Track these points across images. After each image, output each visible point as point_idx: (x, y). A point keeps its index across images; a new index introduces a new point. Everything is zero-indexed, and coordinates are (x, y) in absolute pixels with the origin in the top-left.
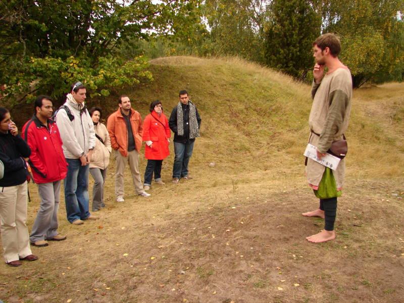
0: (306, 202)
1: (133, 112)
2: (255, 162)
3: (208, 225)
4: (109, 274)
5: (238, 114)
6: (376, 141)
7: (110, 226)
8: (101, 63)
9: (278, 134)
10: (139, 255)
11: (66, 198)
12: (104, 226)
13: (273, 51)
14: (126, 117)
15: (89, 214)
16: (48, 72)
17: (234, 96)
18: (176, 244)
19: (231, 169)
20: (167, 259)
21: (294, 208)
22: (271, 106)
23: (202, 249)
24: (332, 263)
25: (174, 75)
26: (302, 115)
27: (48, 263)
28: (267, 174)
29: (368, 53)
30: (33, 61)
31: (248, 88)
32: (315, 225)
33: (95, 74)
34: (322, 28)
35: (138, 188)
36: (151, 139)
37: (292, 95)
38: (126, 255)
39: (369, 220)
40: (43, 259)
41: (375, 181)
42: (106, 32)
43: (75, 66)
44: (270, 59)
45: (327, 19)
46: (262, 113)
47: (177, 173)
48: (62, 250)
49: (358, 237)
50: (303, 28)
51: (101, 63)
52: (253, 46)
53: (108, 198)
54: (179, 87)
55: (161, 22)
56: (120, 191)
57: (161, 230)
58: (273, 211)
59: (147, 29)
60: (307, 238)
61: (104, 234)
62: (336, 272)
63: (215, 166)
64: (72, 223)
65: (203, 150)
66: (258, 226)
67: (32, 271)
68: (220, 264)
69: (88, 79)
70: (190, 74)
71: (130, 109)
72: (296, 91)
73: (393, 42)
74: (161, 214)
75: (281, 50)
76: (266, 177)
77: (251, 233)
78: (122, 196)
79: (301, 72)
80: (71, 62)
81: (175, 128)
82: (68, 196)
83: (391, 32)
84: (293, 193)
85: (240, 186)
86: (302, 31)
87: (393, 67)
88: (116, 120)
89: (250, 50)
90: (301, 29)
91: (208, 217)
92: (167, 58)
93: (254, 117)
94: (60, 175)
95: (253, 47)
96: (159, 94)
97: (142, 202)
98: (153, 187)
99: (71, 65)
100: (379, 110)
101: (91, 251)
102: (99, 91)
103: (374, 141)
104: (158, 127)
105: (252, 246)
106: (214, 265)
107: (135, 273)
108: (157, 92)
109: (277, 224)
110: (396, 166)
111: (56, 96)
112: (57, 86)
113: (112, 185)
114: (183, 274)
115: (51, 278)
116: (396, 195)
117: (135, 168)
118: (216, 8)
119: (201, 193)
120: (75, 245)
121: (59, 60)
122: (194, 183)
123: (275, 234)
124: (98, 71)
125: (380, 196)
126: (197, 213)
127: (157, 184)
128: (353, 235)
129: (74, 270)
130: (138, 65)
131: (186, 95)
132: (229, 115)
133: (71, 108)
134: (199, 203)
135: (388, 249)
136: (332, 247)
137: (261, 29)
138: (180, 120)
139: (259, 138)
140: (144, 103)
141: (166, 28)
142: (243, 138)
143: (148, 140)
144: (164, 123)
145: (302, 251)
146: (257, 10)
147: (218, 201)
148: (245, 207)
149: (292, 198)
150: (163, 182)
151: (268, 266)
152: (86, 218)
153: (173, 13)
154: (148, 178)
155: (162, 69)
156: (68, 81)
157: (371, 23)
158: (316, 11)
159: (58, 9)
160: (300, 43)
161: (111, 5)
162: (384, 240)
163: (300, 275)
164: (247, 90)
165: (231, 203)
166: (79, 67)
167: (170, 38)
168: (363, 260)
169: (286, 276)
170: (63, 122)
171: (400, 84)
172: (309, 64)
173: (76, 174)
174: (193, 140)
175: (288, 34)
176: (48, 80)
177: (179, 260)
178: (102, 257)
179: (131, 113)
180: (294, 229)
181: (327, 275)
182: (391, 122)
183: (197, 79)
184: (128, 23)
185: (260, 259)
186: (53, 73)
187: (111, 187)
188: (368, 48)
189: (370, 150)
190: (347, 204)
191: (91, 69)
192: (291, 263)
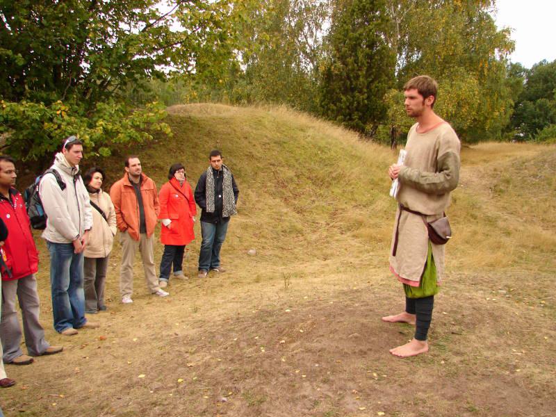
0: (386, 302)
1: (145, 179)
2: (310, 249)
3: (255, 335)
4: (121, 403)
6: (472, 220)
7: (117, 336)
8: (98, 111)
9: (341, 211)
10: (161, 377)
11: (53, 298)
12: (107, 336)
13: (332, 98)
14: (135, 186)
15: (85, 319)
16: (25, 122)
17: (281, 158)
18: (211, 360)
19: (278, 259)
20: (200, 381)
21: (371, 311)
22: (331, 172)
23: (248, 368)
24: (425, 383)
25: (198, 129)
26: (372, 186)
27: (31, 390)
28: (327, 265)
29: (458, 103)
30: (4, 106)
31: (299, 148)
32: (401, 333)
33: (92, 126)
34: (397, 68)
35: (152, 284)
36: (169, 218)
37: (360, 158)
38: (142, 376)
39: (471, 326)
40: (24, 384)
41: (476, 274)
42: (106, 68)
43: (64, 113)
44: (328, 109)
45: (403, 56)
46: (319, 182)
47: (205, 263)
48: (49, 371)
49: (458, 348)
50: (373, 68)
51: (98, 111)
52: (304, 91)
53: (110, 298)
54: (206, 146)
55: (181, 57)
56: (127, 288)
57: (189, 341)
58: (342, 315)
59: (163, 66)
60: (391, 350)
61: (108, 348)
62: (432, 396)
63: (256, 255)
64: (60, 333)
65: (239, 232)
66: (323, 336)
67: (8, 402)
68: (275, 387)
69: (82, 133)
70: (220, 128)
71: (141, 175)
72: (364, 153)
73: (490, 88)
74: (186, 319)
75: (342, 97)
76: (326, 269)
77: (314, 345)
78: (129, 297)
79: (369, 127)
80: (57, 108)
81: (203, 202)
82: (56, 296)
83: (488, 75)
84: (368, 290)
85: (293, 280)
86: (371, 72)
87: (490, 122)
88: (123, 190)
89: (300, 96)
90: (370, 68)
91: (253, 324)
92: (188, 106)
93: (309, 187)
94: (29, 267)
95: (304, 92)
96: (179, 155)
97: (158, 304)
98: (172, 283)
99: (59, 112)
100: (474, 179)
101: (92, 372)
102: (95, 149)
103: (469, 220)
104: (179, 201)
105: (318, 362)
106: (267, 389)
107: (157, 402)
108: (175, 153)
109: (349, 332)
110: (500, 253)
111: (36, 155)
112: (37, 141)
113: (114, 281)
114: (224, 401)
115: (36, 411)
116: (504, 292)
117: (150, 254)
118: (253, 38)
119: (240, 291)
120: (69, 364)
121: (42, 106)
122: (229, 278)
123: (347, 346)
124: (96, 122)
125: (484, 294)
126: (238, 319)
127: (177, 278)
128: (452, 346)
129: (70, 399)
130: (151, 114)
131: (218, 158)
132: (274, 185)
133: (61, 173)
134: (239, 305)
135: (498, 363)
136: (425, 362)
137: (316, 69)
138: (210, 192)
139: (315, 215)
140: (157, 167)
141: (189, 65)
142: (293, 217)
143: (165, 218)
144: (187, 195)
145: (385, 369)
146: (310, 41)
147: (265, 302)
148: (304, 309)
149: (366, 297)
150: (186, 275)
151: (341, 389)
152: (80, 326)
153: (199, 44)
154: (165, 270)
155: (182, 121)
156: (52, 135)
157: (461, 63)
158: (390, 45)
159: (41, 35)
160: (368, 87)
161: (113, 31)
162: (494, 352)
163: (384, 401)
164: (298, 151)
165: (283, 305)
166: (69, 115)
167: (194, 79)
168: (467, 379)
169: (366, 402)
170: (51, 190)
171: (500, 144)
172: (380, 116)
173: (68, 263)
174: (227, 219)
175: (352, 75)
176: (25, 133)
177: (217, 383)
178: (107, 380)
179: (141, 180)
180: (372, 339)
181: (421, 400)
182: (492, 195)
183: (229, 134)
184: (137, 57)
185: (329, 380)
186: (31, 124)
187: (113, 283)
188: (458, 96)
189: (464, 233)
190: (441, 304)
191: (85, 119)
192: (371, 384)
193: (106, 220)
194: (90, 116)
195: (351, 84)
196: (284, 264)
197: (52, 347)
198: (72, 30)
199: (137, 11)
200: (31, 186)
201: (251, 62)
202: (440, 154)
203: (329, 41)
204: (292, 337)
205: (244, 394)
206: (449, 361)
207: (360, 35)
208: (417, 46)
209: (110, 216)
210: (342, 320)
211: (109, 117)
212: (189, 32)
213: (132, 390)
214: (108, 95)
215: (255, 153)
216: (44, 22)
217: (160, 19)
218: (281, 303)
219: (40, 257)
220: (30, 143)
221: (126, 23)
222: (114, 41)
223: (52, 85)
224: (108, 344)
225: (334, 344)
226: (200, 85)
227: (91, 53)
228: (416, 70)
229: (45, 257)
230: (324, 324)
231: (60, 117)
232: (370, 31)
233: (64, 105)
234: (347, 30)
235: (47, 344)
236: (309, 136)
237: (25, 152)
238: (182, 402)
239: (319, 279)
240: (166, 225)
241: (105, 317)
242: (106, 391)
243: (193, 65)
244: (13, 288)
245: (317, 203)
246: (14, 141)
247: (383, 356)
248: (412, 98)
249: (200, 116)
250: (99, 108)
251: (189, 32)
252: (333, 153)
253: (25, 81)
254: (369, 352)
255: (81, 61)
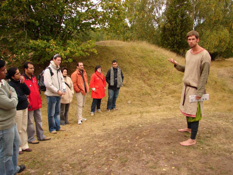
2: (154, 101)
3: (126, 135)
4: (71, 160)
5: (145, 74)
6: (223, 91)
8: (68, 44)
10: (88, 150)
12: (68, 134)
15: (60, 127)
21: (174, 127)
23: (122, 148)
26: (181, 76)
28: (160, 108)
30: (31, 42)
31: (151, 59)
32: (185, 136)
36: (95, 87)
38: (80, 150)
39: (215, 134)
40: (35, 151)
42: (71, 26)
44: (164, 43)
45: (197, 21)
46: (158, 74)
47: (110, 106)
48: (45, 146)
50: (183, 26)
51: (68, 44)
52: (154, 35)
55: (102, 21)
57: (100, 137)
58: (162, 128)
60: (180, 143)
62: (195, 162)
66: (153, 136)
67: (29, 157)
69: (61, 53)
70: (118, 51)
75: (170, 38)
76: (160, 110)
79: (181, 51)
81: (109, 81)
84: (174, 119)
85: (144, 114)
89: (152, 38)
90: (182, 26)
93: (154, 76)
94: (38, 106)
97: (89, 122)
98: (96, 114)
102: (66, 59)
103: (222, 91)
104: (99, 80)
105: (150, 147)
106: (129, 156)
112: (43, 56)
114: (111, 161)
119: (123, 118)
120: (52, 144)
121: (45, 42)
124: (67, 48)
126: (120, 129)
128: (206, 142)
130: (89, 45)
131: (116, 63)
132: (139, 75)
134: (121, 123)
135: (225, 150)
137: (159, 26)
138: (112, 77)
139: (156, 88)
143: (93, 87)
144: (102, 78)
145: (177, 150)
146: (157, 15)
147: (132, 122)
148: (147, 126)
149: (173, 121)
150: (102, 111)
151: (158, 157)
153: (109, 16)
156: (49, 53)
157: (222, 23)
161: (75, 11)
163: (175, 163)
164: (150, 61)
165: (139, 124)
166: (56, 45)
167: (107, 31)
168: (211, 156)
169: (168, 163)
173: (55, 105)
174: (119, 88)
175: (174, 29)
176: (39, 52)
177: (109, 153)
180: (173, 138)
181: (190, 163)
184: (84, 22)
187: (72, 113)
188: (220, 38)
190: (203, 125)
191: (63, 47)
193: (70, 88)
194: (65, 45)
195: (174, 33)
196: (142, 107)
197: (46, 137)
198: (58, 11)
199: (84, 3)
200: (41, 74)
201: (132, 23)
202: (203, 63)
203: (165, 14)
204: (141, 136)
205: (119, 158)
206: (204, 148)
207: (178, 12)
208: (203, 16)
209: (71, 86)
210: (162, 130)
211: (72, 46)
212: (105, 11)
213: (76, 155)
214: (72, 37)
215: (132, 61)
216: (47, 8)
217: (94, 6)
218: (138, 123)
219: (43, 102)
220: (41, 56)
221: (80, 8)
222: (75, 15)
223: (50, 33)
224: (68, 137)
225: (158, 140)
226: (110, 33)
227: (66, 20)
228: (202, 27)
229: (45, 102)
230: (154, 132)
231: (52, 46)
232: (182, 10)
233: (54, 41)
234: (172, 10)
235: (44, 136)
236: (155, 54)
237: (39, 60)
238: (95, 160)
239: (156, 114)
240: (93, 90)
241: (68, 127)
242: (66, 155)
243: (106, 25)
244: (32, 113)
245: (157, 83)
246: (34, 56)
247: (177, 145)
248: (193, 39)
249: (110, 46)
250: (68, 42)
251: (105, 11)
252: (165, 62)
253: (39, 32)
254: (171, 143)
255: (62, 23)
